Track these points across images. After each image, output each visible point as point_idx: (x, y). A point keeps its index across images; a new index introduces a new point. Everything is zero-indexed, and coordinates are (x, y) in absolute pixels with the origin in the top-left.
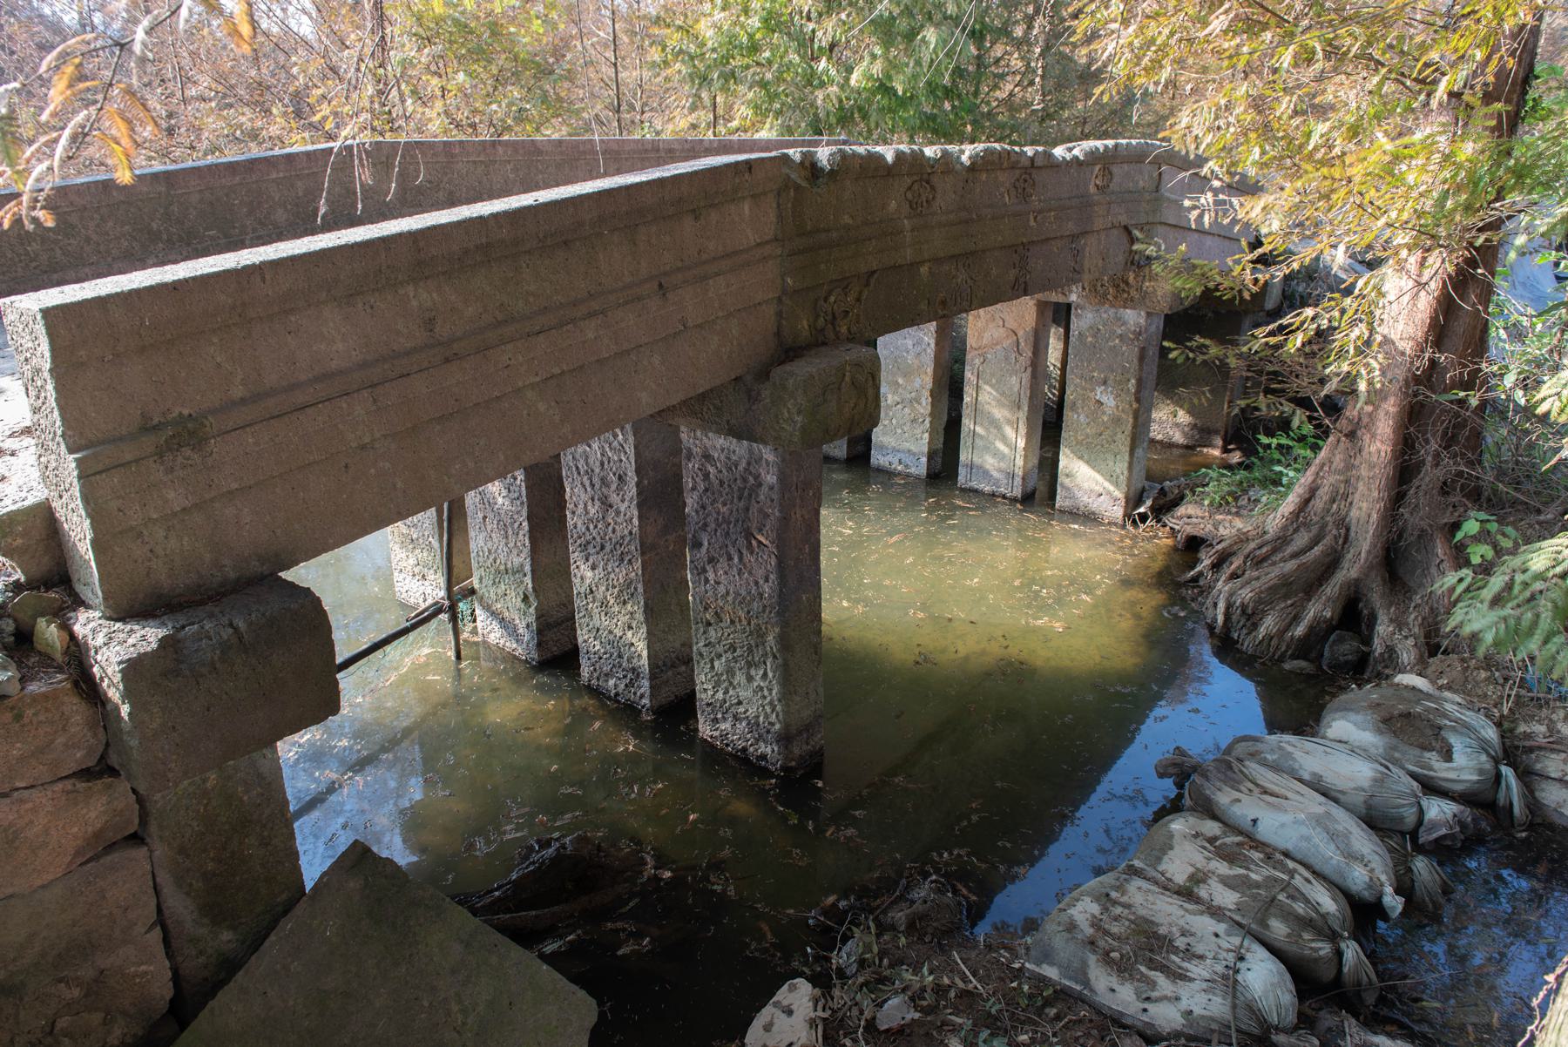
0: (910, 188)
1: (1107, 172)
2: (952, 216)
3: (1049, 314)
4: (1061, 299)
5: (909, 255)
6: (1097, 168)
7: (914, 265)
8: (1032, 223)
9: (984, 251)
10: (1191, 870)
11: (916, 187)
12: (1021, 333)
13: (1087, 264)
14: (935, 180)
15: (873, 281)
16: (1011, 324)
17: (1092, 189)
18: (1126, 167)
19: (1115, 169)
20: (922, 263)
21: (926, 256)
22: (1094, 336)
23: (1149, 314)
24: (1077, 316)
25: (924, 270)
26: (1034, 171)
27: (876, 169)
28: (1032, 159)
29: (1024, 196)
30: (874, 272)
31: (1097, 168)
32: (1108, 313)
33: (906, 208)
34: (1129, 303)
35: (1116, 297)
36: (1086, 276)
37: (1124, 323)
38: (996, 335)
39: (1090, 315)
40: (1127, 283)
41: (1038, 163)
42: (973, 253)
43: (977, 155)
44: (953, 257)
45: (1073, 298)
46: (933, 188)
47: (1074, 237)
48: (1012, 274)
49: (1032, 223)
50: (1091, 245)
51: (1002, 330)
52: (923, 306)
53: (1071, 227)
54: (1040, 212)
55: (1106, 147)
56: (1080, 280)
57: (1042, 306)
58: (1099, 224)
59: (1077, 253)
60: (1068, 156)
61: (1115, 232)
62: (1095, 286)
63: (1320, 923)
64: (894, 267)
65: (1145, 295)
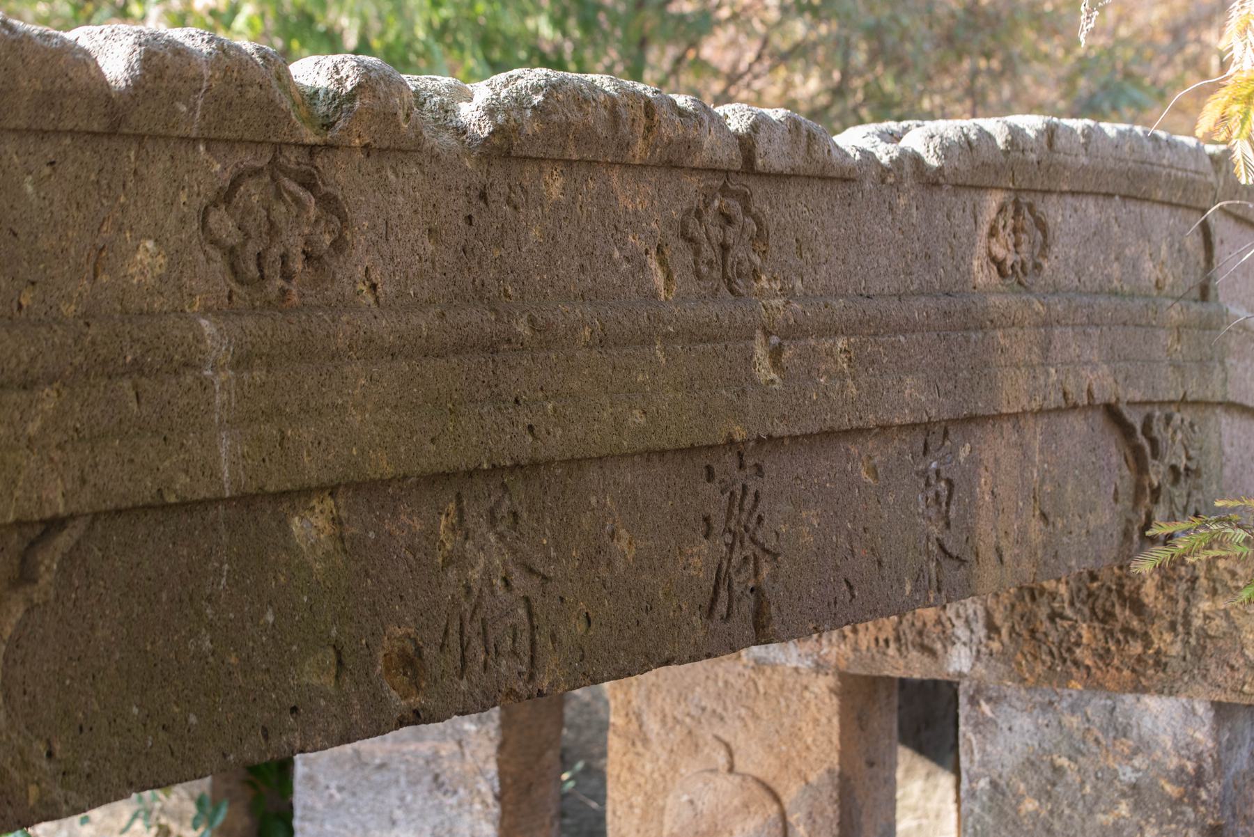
0: (226, 196)
1: (1024, 213)
2: (423, 322)
3: (887, 721)
4: (917, 668)
5: (227, 461)
6: (993, 201)
7: (262, 504)
8: (764, 371)
9: (575, 463)
10: (1113, 400)
11: (253, 192)
12: (791, 792)
13: (987, 533)
14: (341, 175)
15: (48, 563)
16: (755, 760)
17: (982, 274)
18: (1090, 207)
19: (1056, 212)
20: (300, 495)
21: (312, 470)
22: (1044, 794)
23: (1222, 711)
24: (980, 725)
25: (309, 528)
26: (758, 190)
27: (48, 100)
28: (746, 143)
29: (732, 278)
30: (55, 525)
31: (993, 201)
32: (1080, 710)
33: (211, 275)
34: (1150, 674)
35: (1104, 656)
36: (988, 574)
37: (1142, 747)
38: (707, 801)
39: (1023, 722)
40: (1138, 607)
41: (772, 156)
42: (528, 469)
43: (519, 102)
44: (435, 480)
45: (959, 661)
46: (329, 203)
47: (931, 433)
48: (701, 557)
49: (764, 371)
50: (997, 469)
51: (726, 783)
52: (315, 674)
53: (913, 396)
54: (793, 332)
55: (1015, 132)
56: (967, 590)
57: (859, 693)
58: (1014, 392)
59: (948, 494)
60: (884, 153)
61: (1077, 424)
62: (1028, 619)
63: (838, 58)
64: (158, 508)
65: (1203, 649)
